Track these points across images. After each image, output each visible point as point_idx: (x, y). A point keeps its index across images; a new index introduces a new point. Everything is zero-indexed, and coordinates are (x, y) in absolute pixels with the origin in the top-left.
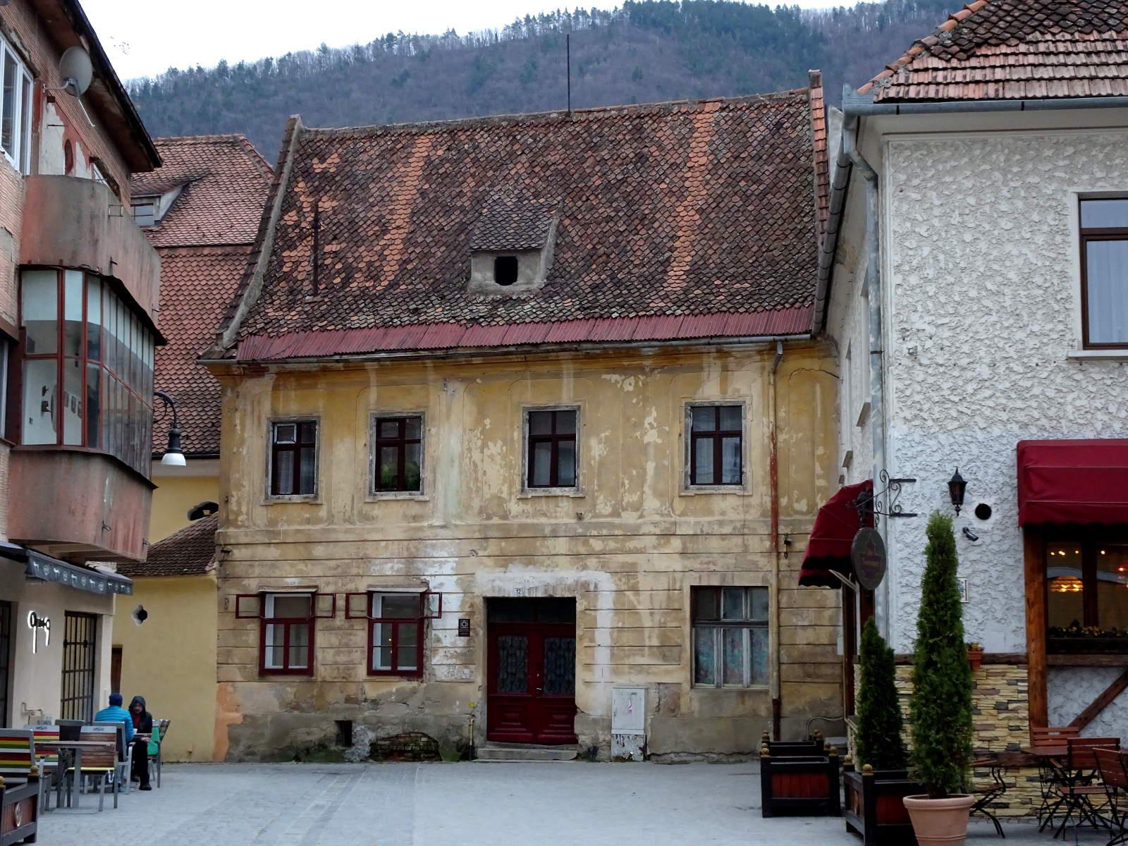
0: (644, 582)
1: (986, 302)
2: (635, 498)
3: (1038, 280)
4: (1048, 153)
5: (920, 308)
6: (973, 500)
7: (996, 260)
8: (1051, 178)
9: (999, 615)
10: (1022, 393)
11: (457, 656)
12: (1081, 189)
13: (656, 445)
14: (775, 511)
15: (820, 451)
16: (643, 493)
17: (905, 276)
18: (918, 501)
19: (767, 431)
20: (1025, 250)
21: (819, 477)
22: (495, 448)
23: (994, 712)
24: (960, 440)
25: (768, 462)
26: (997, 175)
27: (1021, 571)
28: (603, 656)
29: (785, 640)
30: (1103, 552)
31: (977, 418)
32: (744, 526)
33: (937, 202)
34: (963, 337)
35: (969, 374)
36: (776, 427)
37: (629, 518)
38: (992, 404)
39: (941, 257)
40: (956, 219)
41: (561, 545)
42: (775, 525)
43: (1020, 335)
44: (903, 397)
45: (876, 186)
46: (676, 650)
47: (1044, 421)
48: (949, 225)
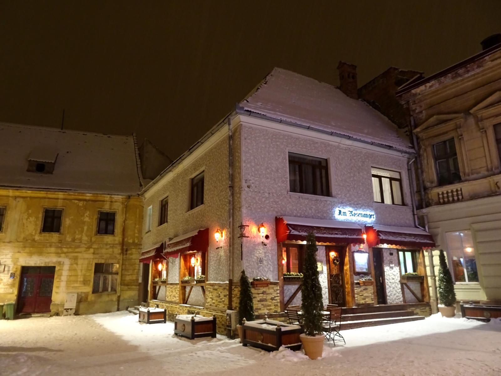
5: (250, 174)
11: (8, 285)
15: (137, 226)
16: (82, 235)
21: (137, 233)
22: (32, 219)
23: (271, 300)
25: (122, 228)
28: (63, 284)
31: (265, 209)
33: (255, 144)
35: (263, 196)
38: (269, 205)
39: (256, 160)
46: (88, 282)
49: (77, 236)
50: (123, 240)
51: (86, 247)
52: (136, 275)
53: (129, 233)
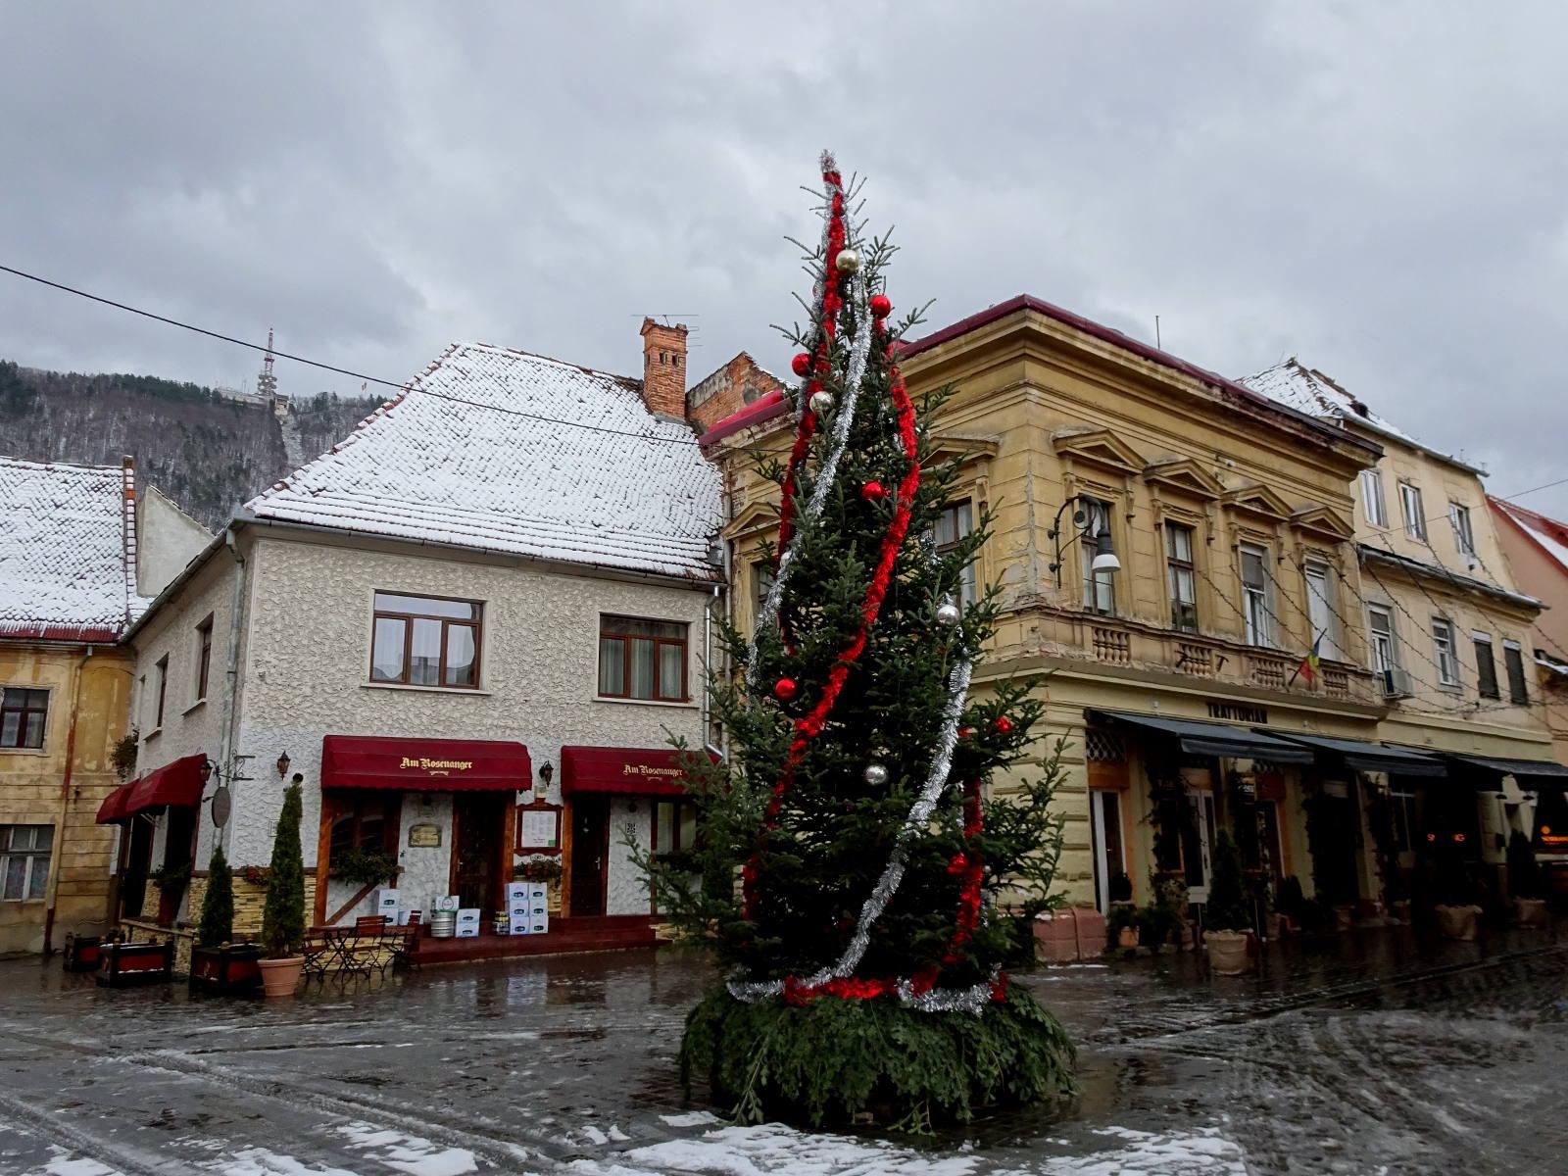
1: (312, 648)
3: (347, 638)
7: (321, 623)
8: (360, 579)
10: (331, 706)
12: (377, 588)
18: (256, 770)
19: (69, 711)
24: (288, 733)
25: (68, 732)
26: (327, 572)
27: (319, 816)
29: (63, 864)
30: (1432, 837)
32: (40, 780)
35: (297, 692)
36: (78, 707)
39: (287, 617)
40: (298, 595)
42: (68, 778)
43: (333, 670)
47: (342, 724)
48: (294, 598)
50: (69, 762)
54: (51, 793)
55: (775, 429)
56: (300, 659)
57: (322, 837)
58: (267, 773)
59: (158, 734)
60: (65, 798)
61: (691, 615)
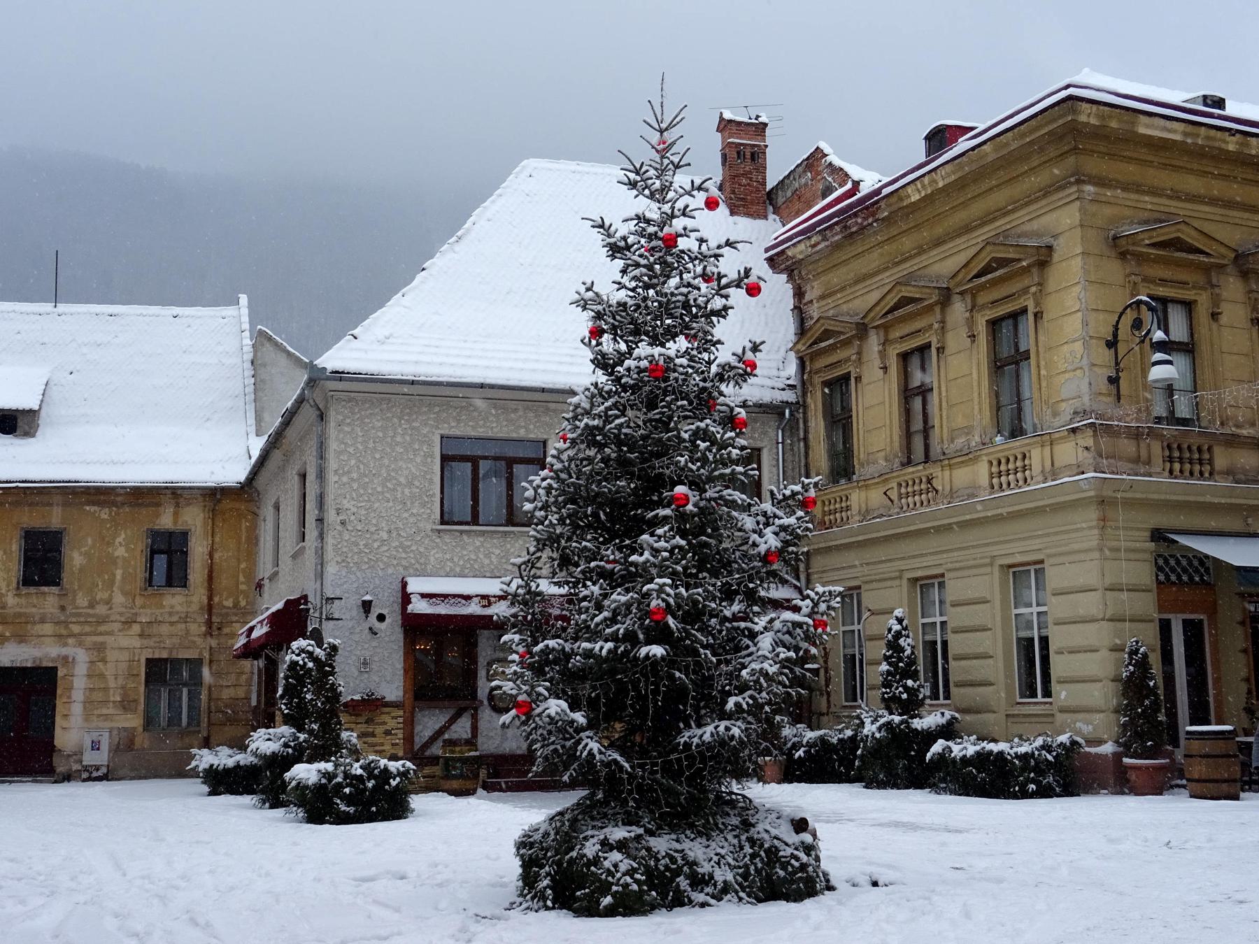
0: (111, 656)
2: (106, 595)
4: (425, 409)
6: (375, 611)
9: (389, 679)
13: (124, 558)
14: (210, 608)
17: (340, 476)
18: (343, 611)
19: (206, 551)
20: (410, 465)
21: (242, 583)
25: (206, 571)
26: (395, 420)
28: (77, 709)
29: (214, 696)
31: (380, 563)
33: (360, 434)
34: (372, 515)
35: (376, 537)
37: (101, 610)
39: (362, 466)
40: (371, 445)
41: (48, 628)
42: (210, 614)
43: (406, 515)
44: (336, 549)
45: (322, 419)
47: (417, 566)
49: (101, 595)
50: (210, 598)
51: (123, 619)
52: (244, 688)
53: (223, 581)
54: (197, 628)
55: (836, 238)
56: (376, 505)
57: (406, 671)
58: (354, 613)
59: (276, 574)
60: (209, 633)
61: (762, 440)
